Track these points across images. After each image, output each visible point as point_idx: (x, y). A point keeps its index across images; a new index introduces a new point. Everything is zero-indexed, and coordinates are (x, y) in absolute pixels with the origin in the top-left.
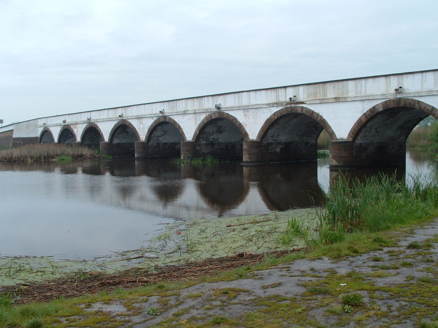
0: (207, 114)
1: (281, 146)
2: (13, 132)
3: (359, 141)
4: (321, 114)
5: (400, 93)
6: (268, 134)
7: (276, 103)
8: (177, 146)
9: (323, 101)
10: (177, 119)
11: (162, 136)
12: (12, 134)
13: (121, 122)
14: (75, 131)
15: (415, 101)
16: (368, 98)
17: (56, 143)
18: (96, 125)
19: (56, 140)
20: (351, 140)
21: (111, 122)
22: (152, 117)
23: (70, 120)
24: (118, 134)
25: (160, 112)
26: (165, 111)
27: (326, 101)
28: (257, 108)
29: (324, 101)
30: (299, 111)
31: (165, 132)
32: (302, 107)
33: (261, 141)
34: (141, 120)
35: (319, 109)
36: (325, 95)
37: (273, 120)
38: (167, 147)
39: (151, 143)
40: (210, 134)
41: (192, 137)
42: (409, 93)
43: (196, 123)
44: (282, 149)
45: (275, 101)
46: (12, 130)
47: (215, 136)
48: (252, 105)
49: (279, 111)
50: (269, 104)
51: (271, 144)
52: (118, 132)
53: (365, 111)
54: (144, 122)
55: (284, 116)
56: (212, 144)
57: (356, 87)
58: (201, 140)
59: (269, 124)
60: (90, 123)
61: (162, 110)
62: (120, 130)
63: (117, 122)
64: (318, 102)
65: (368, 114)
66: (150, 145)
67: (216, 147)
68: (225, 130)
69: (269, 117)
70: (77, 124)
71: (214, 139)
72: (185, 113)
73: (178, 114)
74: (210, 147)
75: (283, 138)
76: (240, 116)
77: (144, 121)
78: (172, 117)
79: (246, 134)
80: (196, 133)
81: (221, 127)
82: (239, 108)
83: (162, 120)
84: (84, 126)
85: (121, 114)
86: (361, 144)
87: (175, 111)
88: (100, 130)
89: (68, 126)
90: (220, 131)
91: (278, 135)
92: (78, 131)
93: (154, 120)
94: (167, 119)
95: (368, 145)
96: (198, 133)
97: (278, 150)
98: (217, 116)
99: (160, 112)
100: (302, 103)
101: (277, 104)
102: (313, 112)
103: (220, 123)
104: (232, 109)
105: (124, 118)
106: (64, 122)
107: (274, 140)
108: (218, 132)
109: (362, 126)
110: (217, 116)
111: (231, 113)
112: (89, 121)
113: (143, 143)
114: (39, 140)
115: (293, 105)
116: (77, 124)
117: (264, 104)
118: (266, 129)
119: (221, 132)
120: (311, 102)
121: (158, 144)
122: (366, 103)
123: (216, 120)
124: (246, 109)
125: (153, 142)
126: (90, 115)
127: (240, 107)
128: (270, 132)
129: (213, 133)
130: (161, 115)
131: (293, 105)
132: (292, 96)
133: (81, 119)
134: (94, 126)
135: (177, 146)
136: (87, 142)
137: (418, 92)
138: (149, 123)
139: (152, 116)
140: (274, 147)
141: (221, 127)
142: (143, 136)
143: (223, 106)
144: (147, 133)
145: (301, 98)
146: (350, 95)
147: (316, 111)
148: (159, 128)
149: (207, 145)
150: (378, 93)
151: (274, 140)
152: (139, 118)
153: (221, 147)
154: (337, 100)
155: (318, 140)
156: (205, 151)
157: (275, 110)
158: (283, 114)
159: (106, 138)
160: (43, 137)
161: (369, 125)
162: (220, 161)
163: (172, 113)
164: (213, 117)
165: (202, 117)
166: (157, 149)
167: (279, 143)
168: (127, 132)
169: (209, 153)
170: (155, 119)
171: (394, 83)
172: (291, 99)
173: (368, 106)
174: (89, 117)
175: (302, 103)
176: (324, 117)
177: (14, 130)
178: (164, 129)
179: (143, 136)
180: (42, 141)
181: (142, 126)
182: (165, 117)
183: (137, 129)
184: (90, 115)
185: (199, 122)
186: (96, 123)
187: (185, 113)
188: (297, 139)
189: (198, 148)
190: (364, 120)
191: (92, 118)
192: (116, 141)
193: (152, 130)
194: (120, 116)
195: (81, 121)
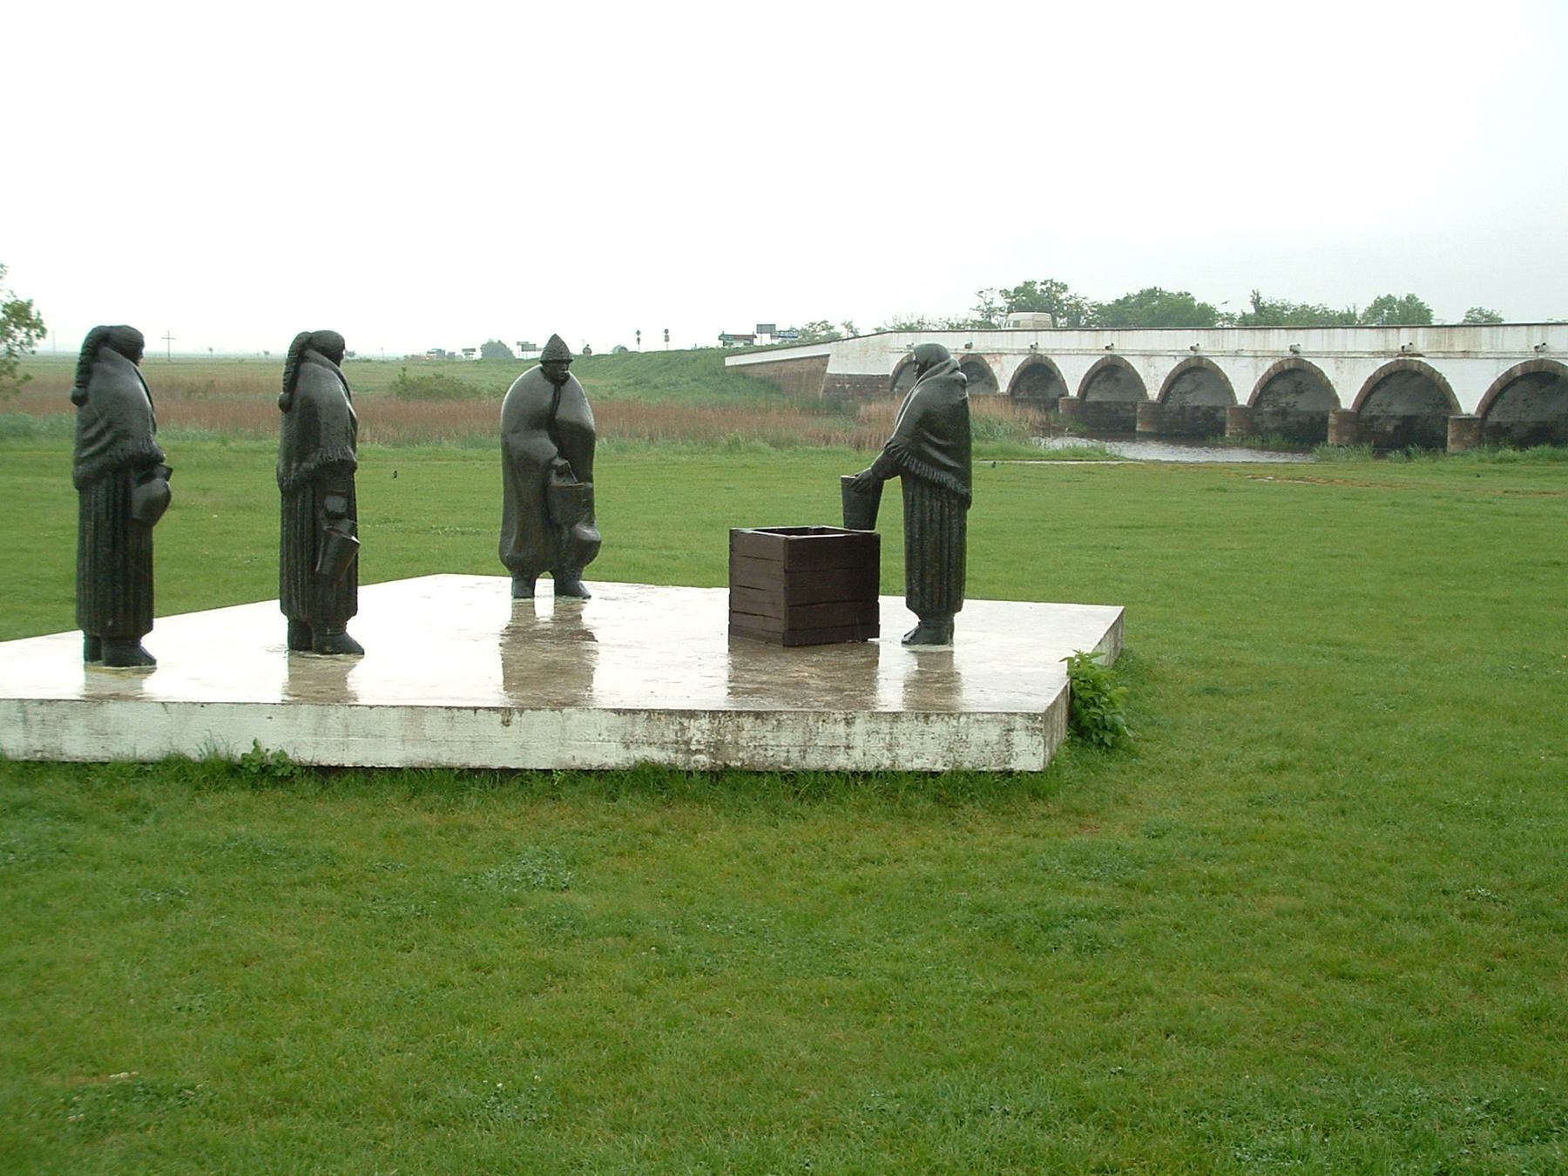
0: (1276, 360)
1: (1395, 422)
2: (827, 361)
3: (1494, 418)
4: (1444, 375)
5: (1542, 352)
6: (1371, 401)
7: (1383, 352)
8: (1220, 414)
9: (1447, 355)
10: (1221, 364)
11: (1191, 392)
12: (825, 365)
13: (1109, 359)
14: (995, 369)
15: (1559, 364)
16: (1504, 356)
17: (1003, 395)
18: (1051, 360)
19: (1004, 387)
20: (1479, 416)
21: (1085, 357)
22: (1175, 357)
23: (983, 345)
24: (1099, 382)
25: (1192, 348)
26: (1201, 346)
27: (1452, 355)
28: (1355, 357)
29: (1448, 355)
30: (1415, 367)
31: (1198, 386)
32: (1420, 362)
33: (1359, 412)
34: (1152, 359)
35: (1439, 366)
36: (1452, 345)
37: (1378, 380)
38: (1199, 414)
39: (1169, 404)
40: (1280, 395)
41: (1248, 399)
42: (1553, 353)
43: (1256, 375)
44: (1396, 428)
45: (1383, 349)
46: (828, 355)
47: (1291, 398)
48: (1349, 352)
49: (1387, 365)
50: (1373, 353)
51: (1377, 418)
52: (1099, 378)
53: (1500, 375)
54: (1157, 364)
55: (1395, 373)
56: (1284, 413)
57: (1491, 338)
58: (1264, 405)
59: (1371, 385)
60: (1035, 354)
61: (1195, 345)
62: (1104, 374)
63: (1099, 358)
64: (1441, 355)
65: (1503, 378)
66: (1167, 410)
67: (1290, 419)
68: (1308, 389)
69: (1372, 373)
70: (1001, 354)
71: (1287, 404)
72: (1237, 354)
73: (1224, 354)
74: (1280, 417)
75: (1399, 409)
76: (1328, 369)
77: (1158, 361)
78: (1214, 360)
79: (1336, 400)
80: (1254, 391)
81: (1300, 383)
82: (1328, 355)
83: (1193, 363)
84: (1022, 359)
85: (1109, 344)
86: (1499, 423)
87: (1220, 349)
88: (1059, 372)
89: (978, 356)
90: (1299, 389)
91: (1390, 404)
92: (1002, 369)
93: (1177, 363)
94: (1204, 361)
95: (1513, 425)
96: (1258, 392)
97: (1389, 428)
98: (1292, 365)
99: (1192, 348)
100: (1420, 355)
101: (1385, 354)
102: (1434, 370)
103: (1298, 377)
104: (1318, 355)
105: (1115, 353)
106: (968, 346)
107: (1383, 411)
108: (1297, 392)
109: (343, 767)
110: (1292, 366)
111: (1315, 362)
112: (1033, 351)
113: (1153, 404)
114: (890, 382)
115: (1407, 358)
116: (1001, 354)
117: (1366, 353)
118: (1366, 392)
119: (1302, 392)
120: (1432, 355)
121: (1182, 407)
122: (1502, 362)
123: (1291, 371)
124: (1339, 357)
125: (1173, 404)
126: (1036, 339)
127: (1329, 353)
128: (1375, 398)
129: (1286, 394)
130: (1192, 353)
131: (1407, 358)
132: (1406, 344)
133: (1012, 344)
134: (1044, 362)
135: (1220, 414)
136: (1021, 396)
137: (1562, 353)
138: (1169, 366)
139: (1175, 354)
140: (1381, 424)
141: (1300, 383)
142: (1153, 392)
143: (1302, 348)
144: (1164, 385)
145: (1420, 347)
146: (1484, 349)
147: (1437, 369)
148: (1187, 376)
149: (1274, 414)
150: (1518, 349)
151: (1383, 411)
152: (1148, 355)
153: (1300, 419)
154: (1466, 354)
155: (1039, 769)
156: (1270, 426)
157: (1382, 362)
158: (1393, 370)
159: (1073, 392)
160: (901, 377)
161: (1507, 394)
162: (525, 589)
163: (1214, 352)
164: (1286, 367)
165: (1268, 365)
166: (1179, 418)
167: (1393, 416)
168: (1117, 380)
169: (1277, 429)
170: (1181, 359)
171: (1537, 337)
172: (1403, 347)
173: (1505, 367)
174: (1034, 344)
175: (1420, 355)
176: (1448, 380)
177: (831, 358)
178: (1196, 378)
179: (1153, 392)
180: (897, 384)
181: (1152, 371)
182: (1200, 358)
183: (1142, 377)
184: (1036, 339)
185: (1261, 374)
186: (1049, 357)
187: (1237, 354)
188: (1427, 411)
189: (1257, 419)
190: (1498, 387)
191: (1040, 346)
192: (1093, 397)
193: (1173, 381)
194: (1107, 348)
195: (1013, 350)
